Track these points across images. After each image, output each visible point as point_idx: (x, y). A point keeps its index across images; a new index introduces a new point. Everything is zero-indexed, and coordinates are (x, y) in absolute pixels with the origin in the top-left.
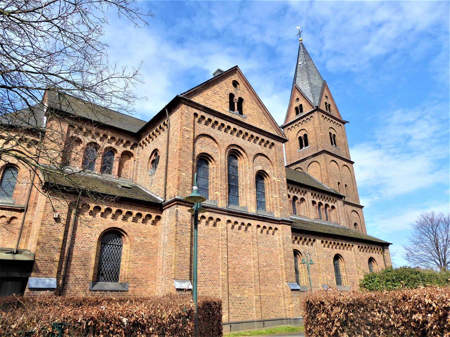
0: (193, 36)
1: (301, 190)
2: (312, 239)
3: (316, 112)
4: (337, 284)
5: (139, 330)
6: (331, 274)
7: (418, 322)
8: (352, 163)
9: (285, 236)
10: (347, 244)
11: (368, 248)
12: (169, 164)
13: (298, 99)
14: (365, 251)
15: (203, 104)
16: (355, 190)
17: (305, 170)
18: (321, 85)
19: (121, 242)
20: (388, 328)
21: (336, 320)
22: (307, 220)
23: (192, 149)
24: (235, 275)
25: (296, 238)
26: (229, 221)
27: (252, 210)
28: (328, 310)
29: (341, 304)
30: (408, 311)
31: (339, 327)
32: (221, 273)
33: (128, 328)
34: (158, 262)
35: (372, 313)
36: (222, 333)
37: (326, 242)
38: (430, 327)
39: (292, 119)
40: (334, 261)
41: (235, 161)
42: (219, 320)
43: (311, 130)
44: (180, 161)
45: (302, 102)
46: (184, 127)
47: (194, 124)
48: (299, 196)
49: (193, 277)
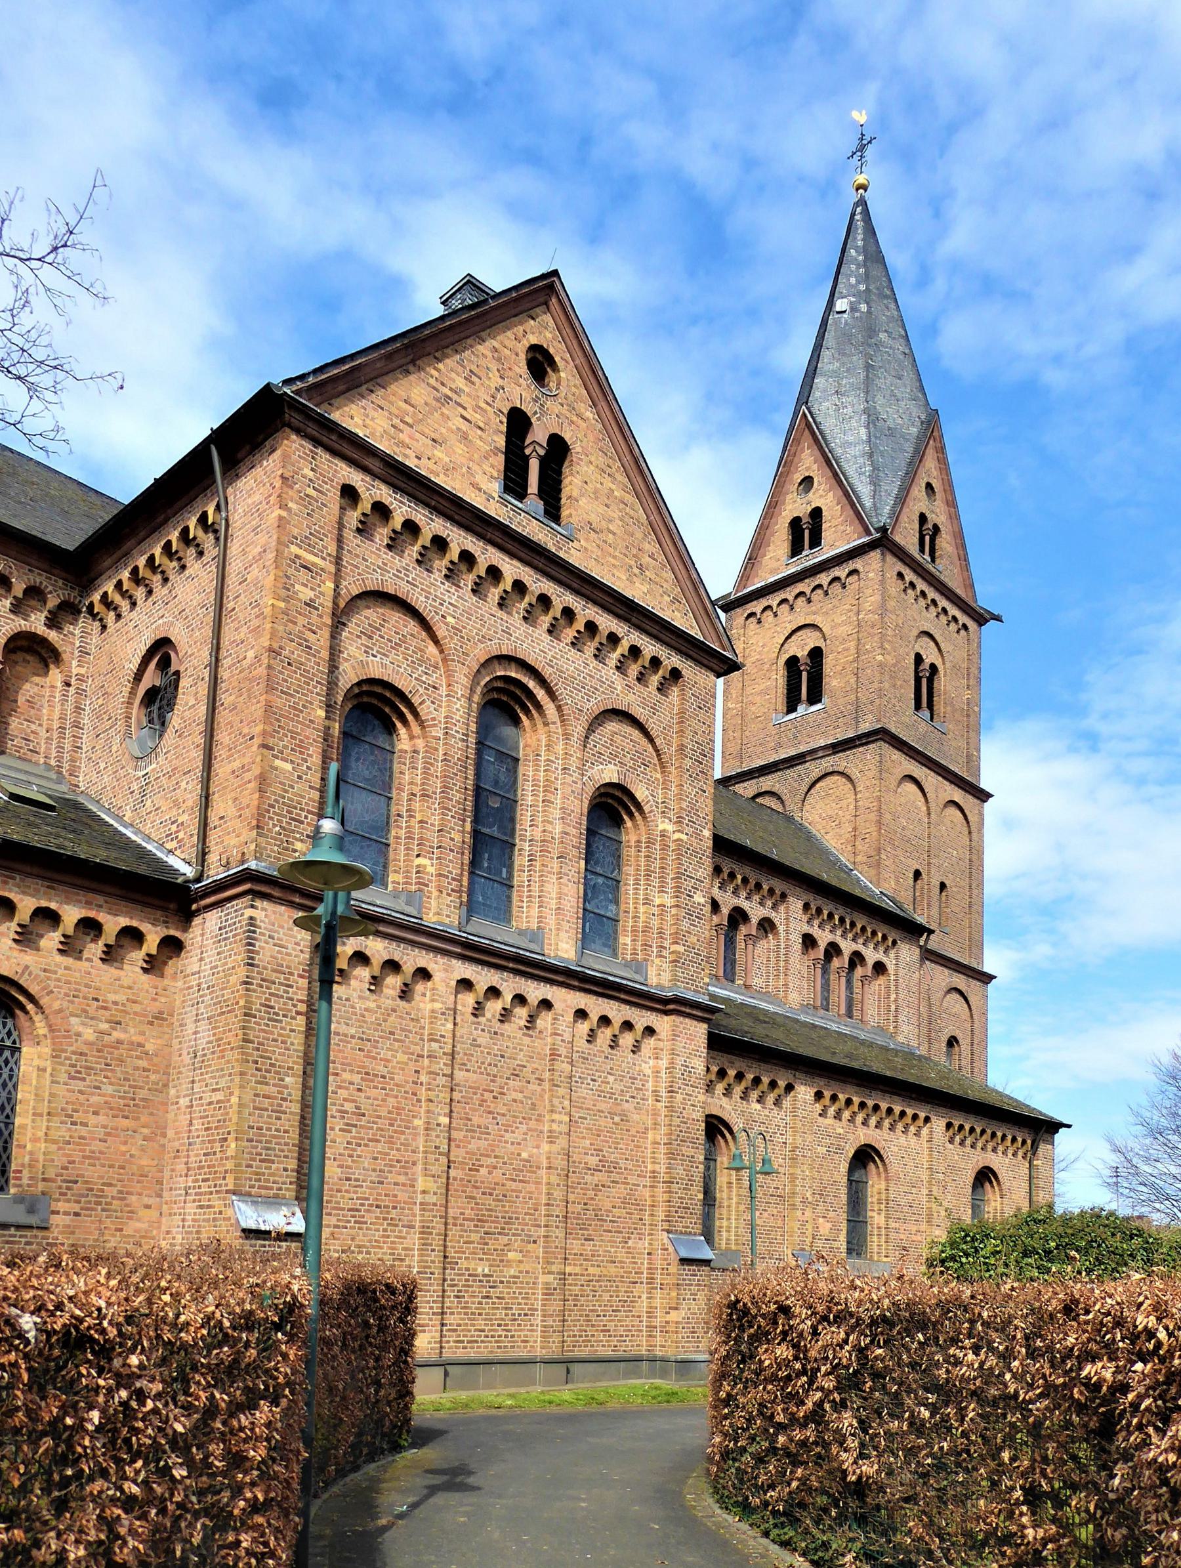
0: (339, 78)
1: (765, 887)
2: (782, 1084)
3: (875, 555)
4: (850, 1251)
5: (88, 1361)
6: (832, 1214)
7: (1097, 1386)
8: (983, 796)
9: (679, 1061)
10: (910, 1112)
11: (983, 1132)
12: (223, 716)
13: (808, 482)
14: (968, 1142)
15: (383, 446)
16: (975, 907)
17: (792, 806)
18: (914, 430)
19: (15, 1034)
20: (994, 1403)
21: (823, 1368)
22: (771, 1008)
23: (325, 654)
24: (477, 1194)
25: (722, 1074)
26: (465, 984)
27: (563, 948)
28: (801, 1335)
29: (851, 1315)
30: (1072, 1349)
31: (830, 1392)
32: (421, 1184)
33: (41, 1354)
34: (170, 1124)
35: (951, 1352)
36: (410, 1393)
37: (834, 1098)
38: (1131, 1405)
39: (774, 571)
40: (851, 1171)
41: (508, 731)
42: (402, 1350)
43: (843, 630)
44: (268, 707)
45: (824, 497)
46: (294, 549)
47: (340, 540)
48: (756, 911)
49: (307, 1189)
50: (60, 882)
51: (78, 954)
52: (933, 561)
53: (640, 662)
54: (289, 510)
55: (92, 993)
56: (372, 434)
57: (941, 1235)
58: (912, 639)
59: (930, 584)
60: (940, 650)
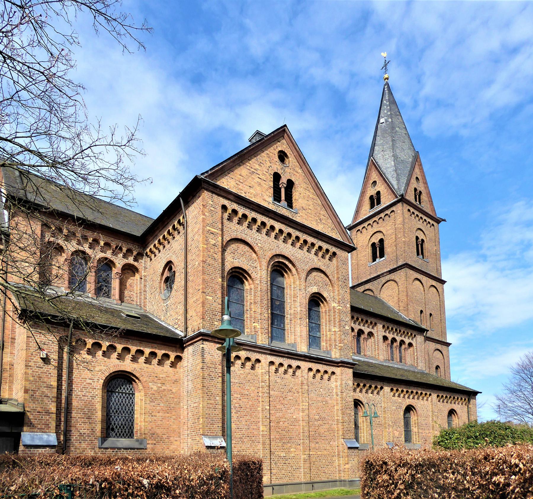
0: (216, 70)
1: (369, 321)
2: (379, 387)
3: (400, 204)
4: (406, 441)
5: (164, 493)
6: (399, 429)
8: (443, 282)
9: (344, 382)
10: (424, 392)
11: (450, 397)
13: (375, 183)
14: (445, 401)
15: (234, 191)
16: (442, 321)
17: (376, 293)
18: (411, 160)
19: (133, 389)
20: (461, 491)
21: (400, 482)
22: (374, 362)
23: (220, 261)
25: (358, 385)
26: (272, 363)
27: (303, 348)
28: (391, 471)
29: (408, 464)
30: (488, 472)
32: (261, 428)
33: (150, 490)
34: (182, 414)
35: (444, 474)
36: (262, 496)
37: (397, 390)
38: (511, 490)
39: (364, 215)
40: (405, 414)
41: (281, 279)
42: (259, 482)
43: (390, 232)
44: (203, 279)
45: (381, 187)
46: (208, 228)
47: (222, 223)
48: (366, 330)
49: (226, 432)
50: (143, 341)
51: (150, 363)
52: (420, 203)
53: (322, 251)
54: (206, 215)
55: (155, 375)
56: (230, 187)
57: (438, 434)
58: (414, 232)
59: (420, 212)
60: (424, 234)
